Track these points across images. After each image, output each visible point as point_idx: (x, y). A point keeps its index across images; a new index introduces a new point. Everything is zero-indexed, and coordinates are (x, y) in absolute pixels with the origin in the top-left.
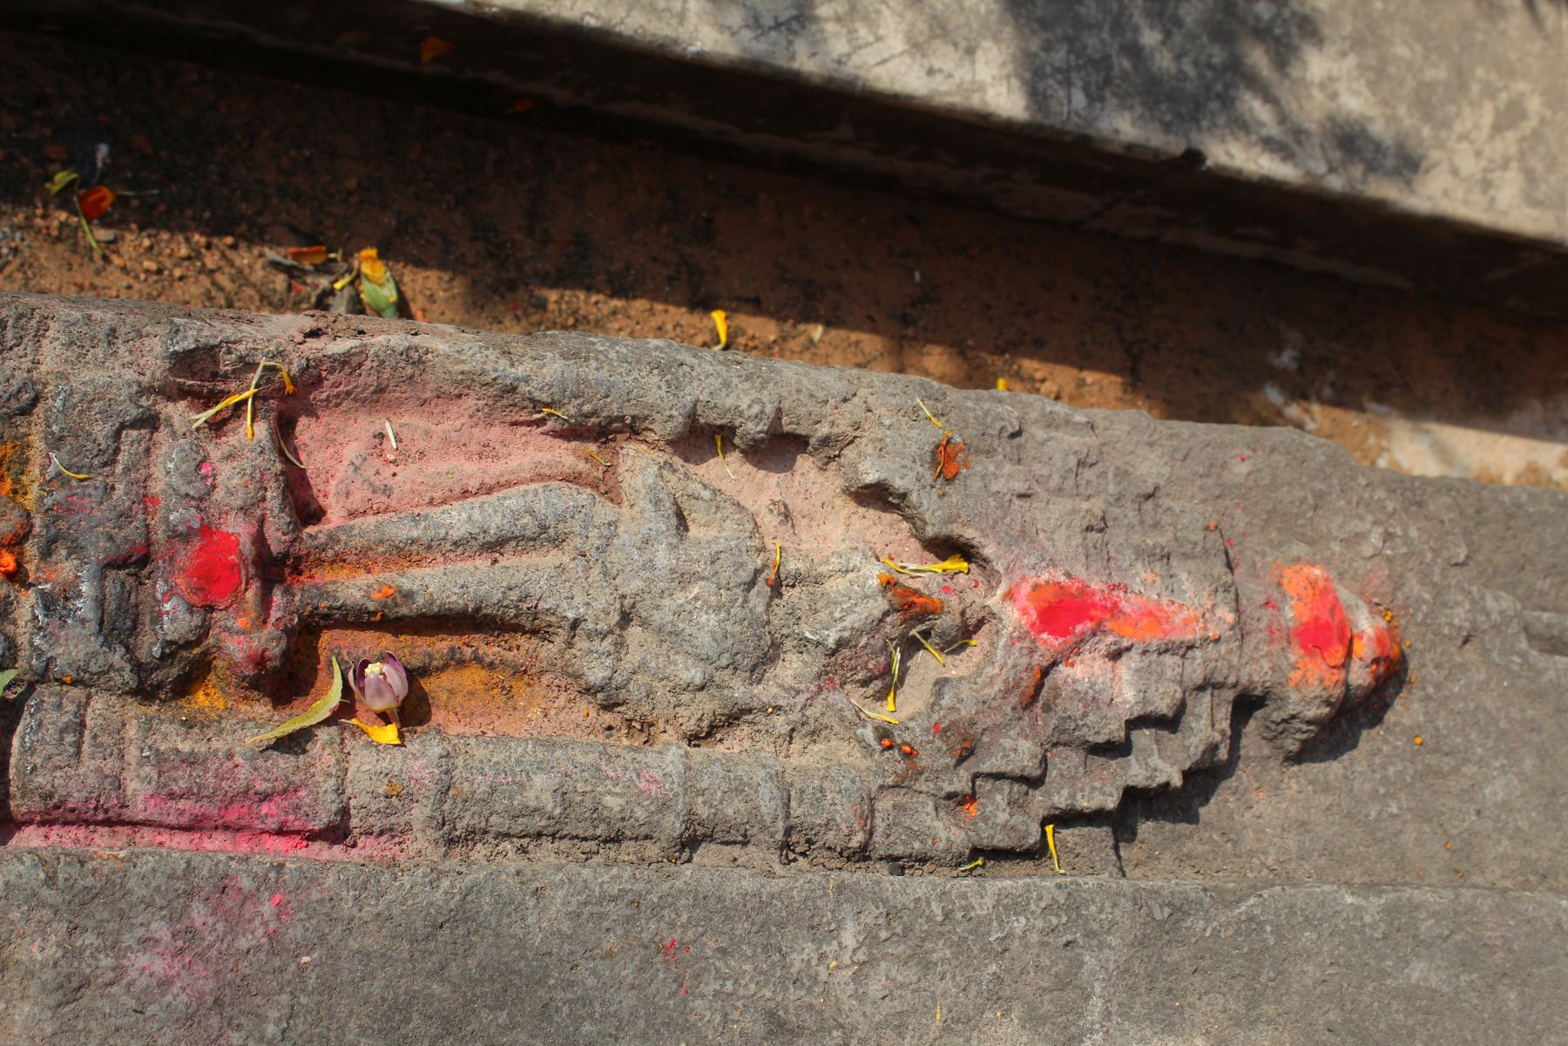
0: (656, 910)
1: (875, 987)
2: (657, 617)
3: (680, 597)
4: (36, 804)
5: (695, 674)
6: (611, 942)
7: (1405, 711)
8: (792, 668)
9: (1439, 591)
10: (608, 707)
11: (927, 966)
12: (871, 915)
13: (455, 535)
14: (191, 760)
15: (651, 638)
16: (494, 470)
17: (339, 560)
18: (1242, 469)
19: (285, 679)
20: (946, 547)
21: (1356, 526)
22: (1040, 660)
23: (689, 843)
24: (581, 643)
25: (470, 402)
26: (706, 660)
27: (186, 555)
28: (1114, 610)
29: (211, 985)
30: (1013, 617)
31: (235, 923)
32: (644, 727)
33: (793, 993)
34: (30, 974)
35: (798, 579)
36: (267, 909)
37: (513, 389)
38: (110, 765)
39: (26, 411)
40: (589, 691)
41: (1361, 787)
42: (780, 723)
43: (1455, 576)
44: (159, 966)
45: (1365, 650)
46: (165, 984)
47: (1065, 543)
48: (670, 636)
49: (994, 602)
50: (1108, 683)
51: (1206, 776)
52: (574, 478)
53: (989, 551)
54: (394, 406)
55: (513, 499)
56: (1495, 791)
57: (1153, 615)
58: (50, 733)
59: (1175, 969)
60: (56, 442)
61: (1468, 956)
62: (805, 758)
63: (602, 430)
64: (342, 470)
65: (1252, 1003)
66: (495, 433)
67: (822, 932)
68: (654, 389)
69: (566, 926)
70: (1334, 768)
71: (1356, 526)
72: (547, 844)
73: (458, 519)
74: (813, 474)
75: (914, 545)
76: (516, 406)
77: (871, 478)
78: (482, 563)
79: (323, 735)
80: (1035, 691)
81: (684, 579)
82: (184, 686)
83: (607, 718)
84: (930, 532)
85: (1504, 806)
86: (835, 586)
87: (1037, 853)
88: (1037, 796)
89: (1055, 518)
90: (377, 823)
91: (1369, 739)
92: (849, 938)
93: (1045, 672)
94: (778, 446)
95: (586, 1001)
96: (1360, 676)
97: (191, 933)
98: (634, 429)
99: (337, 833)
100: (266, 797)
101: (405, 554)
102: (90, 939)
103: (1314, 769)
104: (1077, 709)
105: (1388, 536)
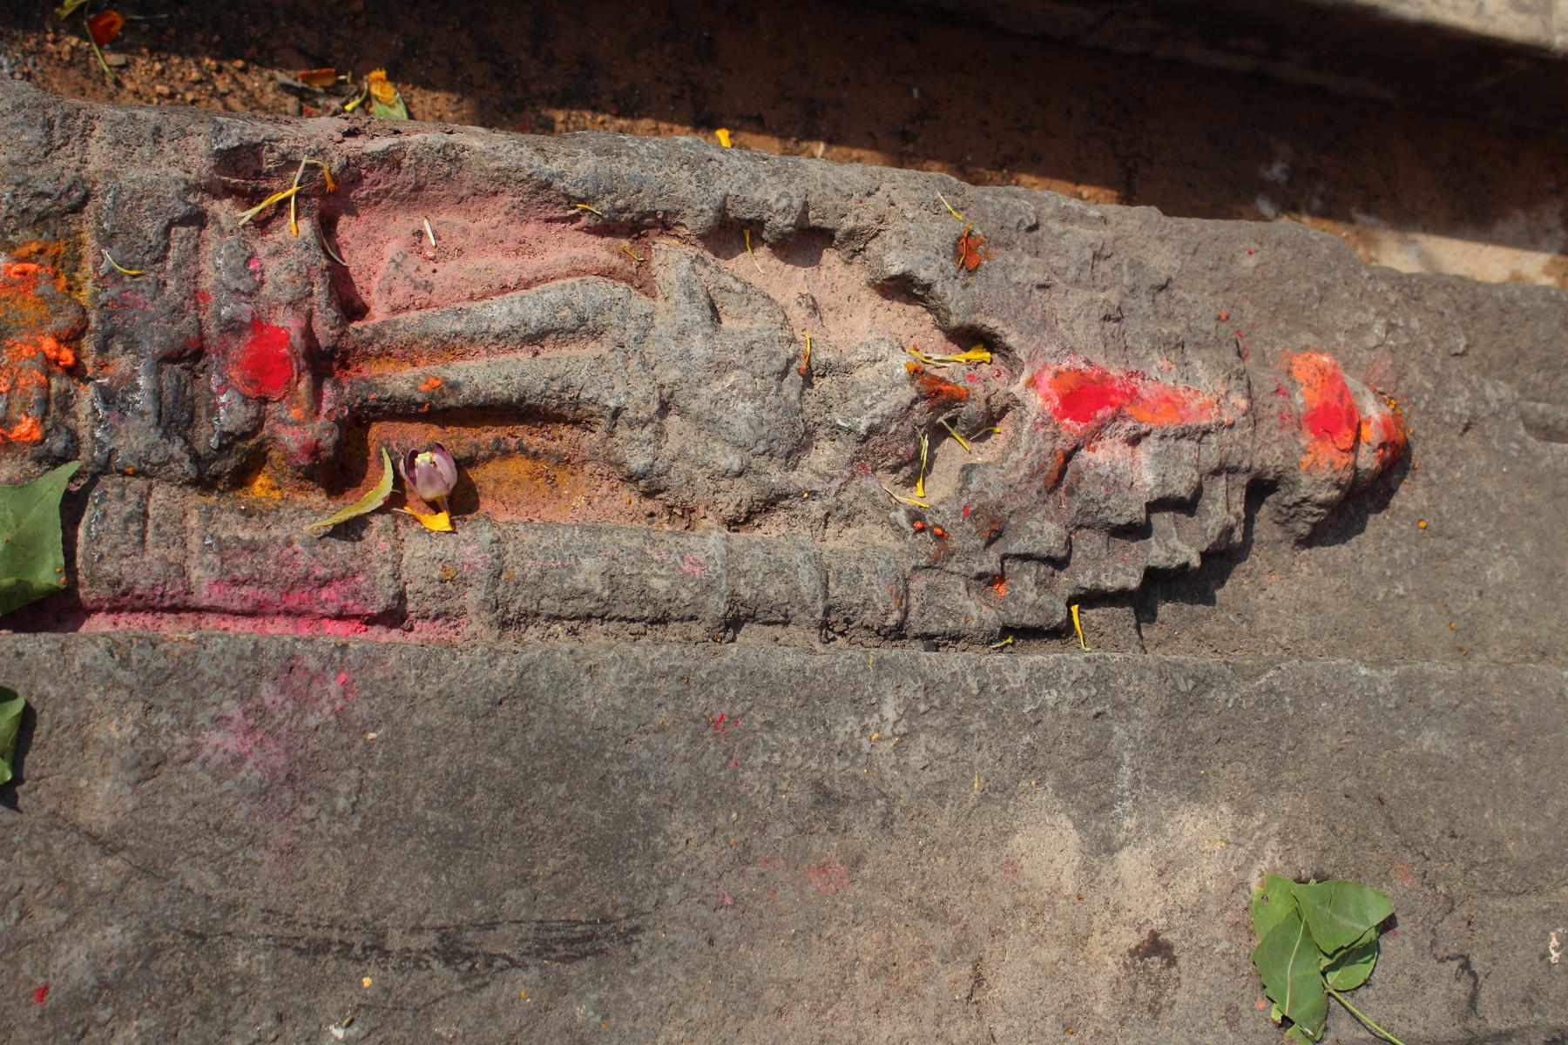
0: (705, 685)
1: (916, 758)
2: (694, 406)
3: (717, 386)
4: (105, 591)
5: (733, 461)
6: (662, 716)
7: (1409, 497)
8: (824, 455)
9: (1440, 380)
10: (649, 494)
11: (964, 737)
12: (910, 688)
13: (497, 327)
14: (252, 548)
15: (689, 427)
16: (530, 266)
17: (385, 354)
18: (1251, 262)
19: (338, 470)
20: (969, 337)
21: (1360, 317)
22: (1062, 445)
23: (733, 623)
24: (623, 432)
25: (506, 200)
26: (743, 446)
27: (238, 348)
28: (1133, 396)
29: (281, 761)
30: (1036, 403)
31: (303, 702)
32: (685, 514)
33: (839, 765)
34: (109, 751)
35: (828, 369)
36: (334, 687)
37: (547, 185)
38: (174, 554)
39: (77, 209)
40: (631, 478)
41: (1370, 569)
42: (816, 508)
43: (1456, 366)
44: (232, 743)
45: (1372, 435)
46: (239, 760)
47: (1085, 331)
48: (708, 424)
49: (1017, 389)
50: (1129, 467)
51: (1223, 558)
52: (609, 273)
53: (1012, 340)
54: (432, 205)
55: (552, 293)
56: (1496, 572)
57: (1170, 401)
58: (115, 522)
59: (1199, 740)
60: (108, 239)
61: (1475, 726)
62: (840, 542)
63: (635, 226)
64: (384, 267)
65: (1273, 771)
66: (531, 229)
67: (864, 706)
68: (684, 184)
69: (619, 702)
70: (1343, 551)
71: (1360, 317)
72: (596, 626)
73: (499, 313)
74: (839, 268)
75: (938, 335)
76: (552, 203)
77: (896, 270)
78: (524, 355)
79: (378, 522)
80: (1058, 475)
81: (720, 368)
82: (241, 478)
83: (649, 505)
84: (954, 321)
85: (1506, 587)
86: (865, 375)
87: (1062, 632)
88: (1063, 577)
89: (1074, 308)
90: (433, 607)
91: (1376, 523)
92: (890, 710)
93: (1068, 457)
94: (805, 241)
95: (640, 773)
96: (1368, 460)
97: (262, 711)
98: (665, 224)
99: (394, 617)
100: (325, 582)
101: (448, 347)
102: (165, 718)
103: (1323, 552)
104: (1099, 492)
105: (1391, 327)
